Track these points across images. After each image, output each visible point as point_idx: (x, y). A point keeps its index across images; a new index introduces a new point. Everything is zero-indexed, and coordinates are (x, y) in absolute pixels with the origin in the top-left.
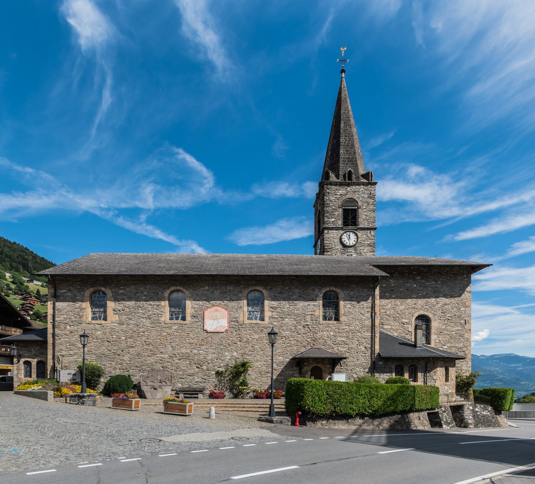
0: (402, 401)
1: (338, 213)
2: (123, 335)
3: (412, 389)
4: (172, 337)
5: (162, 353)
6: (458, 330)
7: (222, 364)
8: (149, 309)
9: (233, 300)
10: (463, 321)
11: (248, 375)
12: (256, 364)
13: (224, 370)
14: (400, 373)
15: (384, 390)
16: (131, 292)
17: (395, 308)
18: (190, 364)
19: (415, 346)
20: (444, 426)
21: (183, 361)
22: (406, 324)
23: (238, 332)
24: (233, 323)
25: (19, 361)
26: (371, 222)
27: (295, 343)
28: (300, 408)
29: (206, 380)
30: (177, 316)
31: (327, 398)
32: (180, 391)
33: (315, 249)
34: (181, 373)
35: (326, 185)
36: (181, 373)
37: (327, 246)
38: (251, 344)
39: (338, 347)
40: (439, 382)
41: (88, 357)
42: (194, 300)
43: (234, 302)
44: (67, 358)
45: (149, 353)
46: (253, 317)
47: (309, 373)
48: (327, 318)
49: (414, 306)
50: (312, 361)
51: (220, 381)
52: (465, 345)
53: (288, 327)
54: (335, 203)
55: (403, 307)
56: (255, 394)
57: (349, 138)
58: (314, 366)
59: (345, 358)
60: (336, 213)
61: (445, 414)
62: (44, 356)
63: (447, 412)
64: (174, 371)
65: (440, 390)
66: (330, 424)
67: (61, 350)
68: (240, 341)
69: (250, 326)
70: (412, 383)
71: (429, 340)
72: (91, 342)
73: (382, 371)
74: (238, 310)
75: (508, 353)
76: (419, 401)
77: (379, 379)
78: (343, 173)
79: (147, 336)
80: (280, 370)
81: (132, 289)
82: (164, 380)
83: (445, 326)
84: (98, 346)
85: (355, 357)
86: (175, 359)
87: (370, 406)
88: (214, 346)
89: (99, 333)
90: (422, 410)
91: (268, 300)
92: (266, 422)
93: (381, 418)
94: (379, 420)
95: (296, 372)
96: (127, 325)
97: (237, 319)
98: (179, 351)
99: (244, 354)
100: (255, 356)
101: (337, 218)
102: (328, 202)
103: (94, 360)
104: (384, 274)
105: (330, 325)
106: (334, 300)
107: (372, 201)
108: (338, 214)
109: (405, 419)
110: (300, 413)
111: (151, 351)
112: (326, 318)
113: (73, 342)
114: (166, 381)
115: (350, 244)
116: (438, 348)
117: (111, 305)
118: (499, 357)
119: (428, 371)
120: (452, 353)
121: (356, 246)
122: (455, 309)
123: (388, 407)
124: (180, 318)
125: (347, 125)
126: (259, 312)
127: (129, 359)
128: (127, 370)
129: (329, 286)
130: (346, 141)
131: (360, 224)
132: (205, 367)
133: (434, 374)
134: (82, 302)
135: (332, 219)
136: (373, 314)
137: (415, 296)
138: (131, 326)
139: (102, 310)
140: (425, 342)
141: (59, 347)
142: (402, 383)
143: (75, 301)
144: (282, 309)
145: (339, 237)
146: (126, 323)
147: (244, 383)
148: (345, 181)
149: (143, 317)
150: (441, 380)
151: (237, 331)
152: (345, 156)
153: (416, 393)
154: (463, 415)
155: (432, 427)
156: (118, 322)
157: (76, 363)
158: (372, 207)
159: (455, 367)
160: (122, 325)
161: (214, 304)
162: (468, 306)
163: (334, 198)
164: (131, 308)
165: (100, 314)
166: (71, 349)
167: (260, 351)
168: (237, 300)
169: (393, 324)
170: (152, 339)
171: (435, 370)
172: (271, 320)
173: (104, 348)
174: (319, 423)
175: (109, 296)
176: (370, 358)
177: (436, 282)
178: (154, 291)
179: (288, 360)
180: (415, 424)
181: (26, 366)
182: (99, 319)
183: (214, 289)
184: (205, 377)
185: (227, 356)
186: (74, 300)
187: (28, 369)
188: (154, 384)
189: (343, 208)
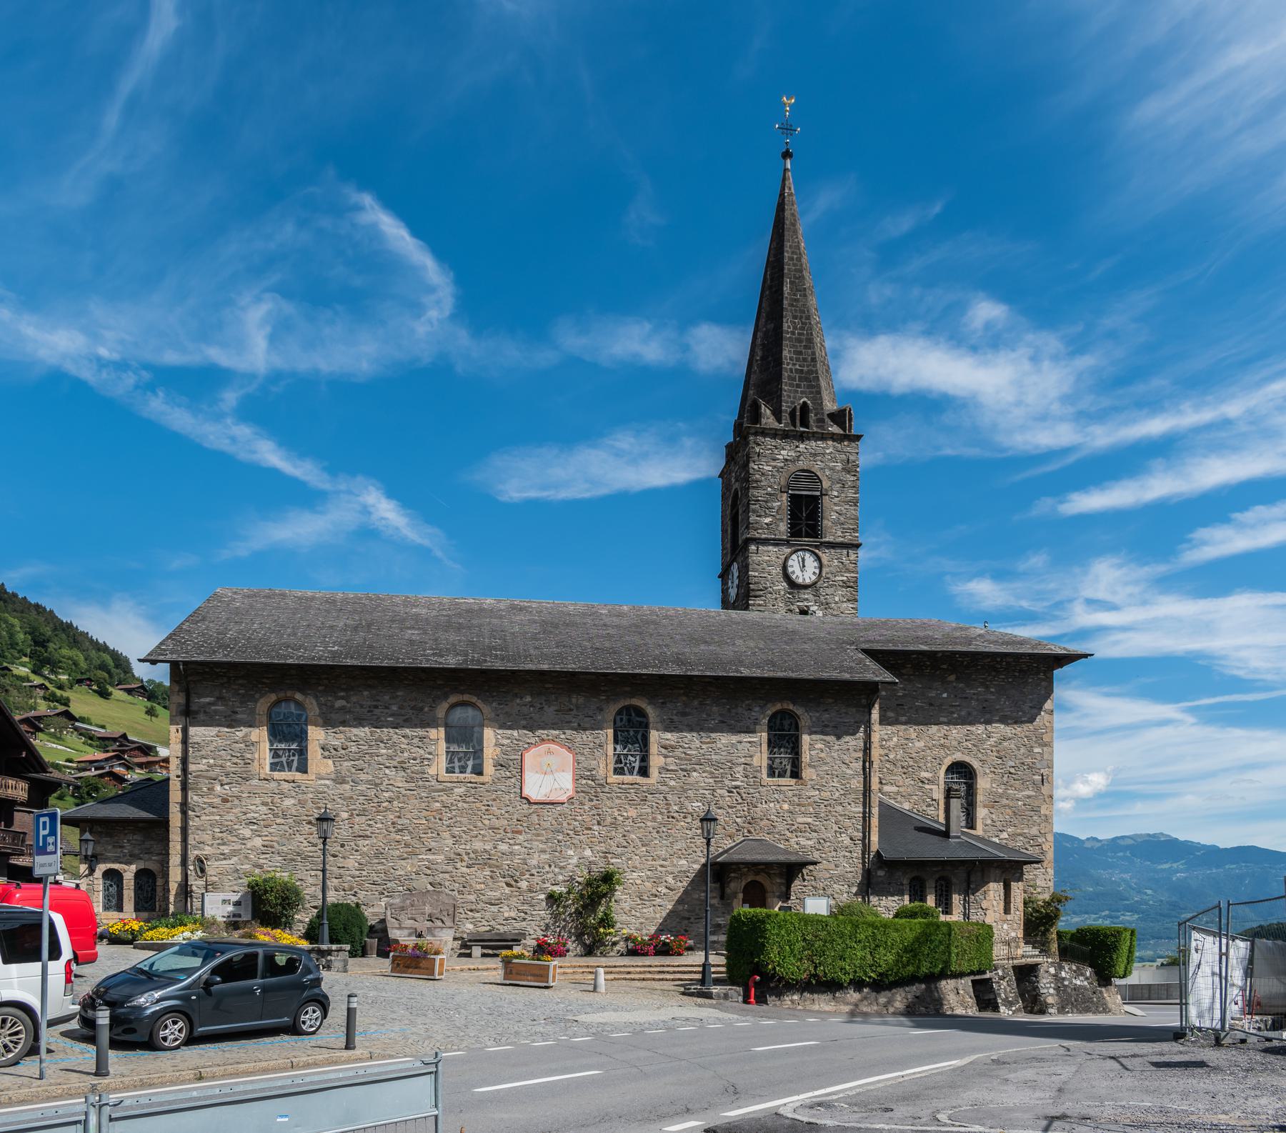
0: (928, 955)
1: (779, 503)
2: (345, 809)
3: (945, 929)
4: (454, 813)
5: (430, 850)
6: (1029, 797)
7: (561, 878)
8: (403, 746)
9: (585, 729)
10: (1038, 778)
11: (616, 901)
12: (631, 877)
13: (564, 890)
14: (918, 895)
15: (897, 930)
16: (362, 706)
17: (905, 747)
18: (492, 877)
19: (946, 834)
20: (1002, 1009)
21: (476, 869)
22: (926, 782)
23: (595, 802)
24: (584, 782)
25: (92, 871)
26: (849, 529)
28: (758, 969)
29: (526, 913)
30: (462, 763)
31: (803, 947)
32: (470, 941)
33: (724, 583)
34: (472, 898)
35: (752, 434)
36: (472, 898)
37: (755, 583)
38: (621, 830)
39: (797, 837)
40: (993, 914)
41: (264, 861)
42: (501, 727)
43: (587, 732)
44: (216, 863)
45: (402, 850)
46: (626, 768)
47: (741, 896)
48: (777, 771)
49: (942, 741)
51: (556, 917)
52: (1042, 832)
54: (772, 480)
55: (921, 744)
56: (631, 945)
57: (802, 323)
59: (815, 863)
60: (775, 504)
61: (1004, 983)
62: (153, 858)
63: (1007, 979)
64: (457, 894)
65: (995, 930)
66: (805, 1000)
67: (201, 843)
68: (599, 824)
69: (619, 788)
70: (943, 918)
71: (972, 819)
72: (271, 823)
73: (884, 892)
75: (1151, 833)
76: (957, 954)
77: (879, 909)
78: (789, 407)
79: (398, 809)
80: (682, 890)
81: (364, 697)
82: (438, 916)
83: (1003, 787)
84: (287, 834)
85: (831, 859)
86: (458, 865)
87: (873, 965)
88: (543, 835)
89: (289, 802)
90: (961, 975)
91: (658, 730)
93: (890, 990)
94: (888, 993)
96: (353, 784)
98: (468, 848)
100: (630, 859)
101: (778, 517)
102: (757, 476)
103: (276, 866)
104: (887, 677)
105: (783, 788)
107: (852, 478)
108: (780, 507)
109: (931, 992)
110: (758, 978)
111: (407, 845)
112: (774, 772)
113: (230, 823)
114: (444, 919)
116: (991, 839)
117: (316, 735)
118: (1130, 842)
119: (973, 889)
120: (1017, 848)
121: (818, 585)
122: (1023, 750)
123: (904, 966)
124: (469, 769)
125: (797, 290)
126: (638, 757)
127: (356, 864)
128: (352, 892)
129: (781, 700)
130: (795, 328)
131: (826, 534)
132: (524, 885)
134: (250, 726)
135: (765, 517)
136: (867, 764)
137: (945, 720)
138: (362, 787)
139: (294, 746)
140: (963, 824)
141: (197, 837)
142: (925, 918)
143: (233, 723)
144: (685, 750)
145: (781, 561)
146: (350, 779)
147: (607, 921)
148: (795, 426)
149: (388, 765)
150: (996, 909)
151: (592, 800)
152: (794, 365)
153: (952, 938)
154: (1037, 987)
155: (980, 1011)
156: (333, 776)
157: (236, 875)
158: (850, 494)
159: (1022, 881)
160: (341, 783)
161: (544, 737)
162: (1048, 745)
163: (770, 468)
164: (362, 742)
165: (289, 756)
166: (226, 840)
167: (640, 845)
168: (593, 729)
169: (901, 784)
170: (410, 817)
171: (985, 888)
173: (302, 840)
174: (787, 999)
175: (312, 714)
177: (987, 687)
178: (414, 703)
179: (697, 867)
180: (950, 1004)
181: (108, 882)
182: (286, 769)
183: (543, 701)
184: (526, 907)
185: (571, 857)
186: (232, 723)
187: (113, 890)
188: (416, 925)
189: (790, 492)
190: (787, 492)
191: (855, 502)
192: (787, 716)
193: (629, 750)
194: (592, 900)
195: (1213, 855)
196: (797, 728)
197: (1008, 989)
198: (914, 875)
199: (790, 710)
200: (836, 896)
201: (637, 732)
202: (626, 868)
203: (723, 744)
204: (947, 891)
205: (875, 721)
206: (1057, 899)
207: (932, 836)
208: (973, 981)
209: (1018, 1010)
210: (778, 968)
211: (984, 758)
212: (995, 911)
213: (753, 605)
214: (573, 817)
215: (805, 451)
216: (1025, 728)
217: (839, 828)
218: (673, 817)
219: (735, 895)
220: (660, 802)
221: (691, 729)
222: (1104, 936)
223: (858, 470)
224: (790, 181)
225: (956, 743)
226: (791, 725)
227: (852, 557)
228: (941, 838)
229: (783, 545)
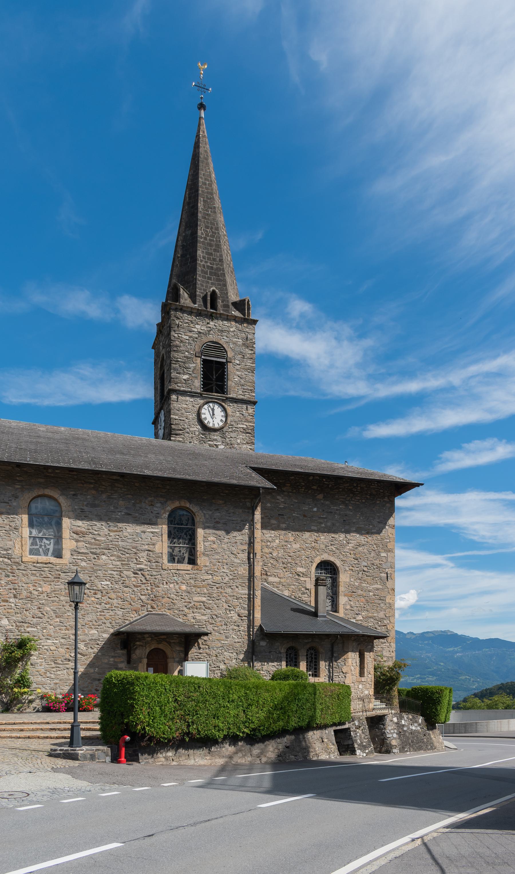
0: (296, 711)
1: (194, 365)
6: (378, 589)
11: (32, 664)
12: (46, 644)
14: (293, 661)
15: (268, 691)
17: (285, 547)
19: (315, 614)
20: (358, 752)
22: (301, 575)
23: (11, 578)
26: (248, 390)
27: (120, 603)
28: (128, 729)
31: (175, 707)
33: (156, 428)
37: (176, 424)
38: (36, 603)
39: (193, 612)
40: (351, 677)
46: (41, 550)
47: (145, 661)
48: (176, 558)
49: (313, 544)
50: (150, 639)
52: (387, 615)
54: (189, 347)
55: (297, 546)
56: (44, 702)
57: (213, 232)
58: (153, 648)
59: (206, 634)
60: (191, 365)
61: (359, 731)
63: (362, 728)
65: (352, 690)
66: (180, 756)
68: (15, 597)
69: (34, 566)
70: (312, 680)
74: (11, 532)
76: (322, 710)
77: (262, 672)
78: (202, 293)
80: (93, 655)
83: (359, 581)
85: (222, 632)
87: (246, 722)
90: (325, 727)
91: (69, 518)
92: (64, 758)
94: (261, 745)
95: (122, 660)
99: (23, 622)
100: (45, 628)
101: (193, 375)
104: (268, 485)
105: (181, 572)
106: (187, 525)
107: (250, 352)
108: (195, 368)
109: (300, 742)
112: (174, 559)
116: (349, 620)
118: (432, 635)
119: (336, 657)
121: (225, 430)
122: (373, 554)
126: (52, 541)
130: (207, 235)
135: (184, 374)
137: (316, 528)
140: (329, 608)
144: (94, 536)
145: (196, 409)
147: (22, 682)
148: (207, 309)
150: (353, 673)
151: (8, 576)
152: (206, 262)
153: (317, 696)
154: (384, 733)
155: (341, 755)
158: (249, 363)
159: (373, 652)
162: (391, 551)
163: (187, 337)
168: (9, 514)
169: (282, 576)
171: (345, 656)
172: (75, 557)
174: (161, 756)
176: (247, 634)
177: (346, 505)
179: (106, 636)
180: (315, 751)
189: (203, 357)
190: (201, 357)
191: (252, 370)
194: (8, 663)
195: (476, 643)
196: (193, 524)
197: (363, 736)
198: (289, 645)
200: (226, 662)
202: (41, 636)
203: (128, 533)
204: (316, 658)
205: (258, 521)
206: (398, 666)
207: (304, 615)
208: (335, 731)
209: (371, 752)
210: (147, 728)
212: (352, 675)
216: (375, 538)
217: (229, 606)
219: (140, 660)
221: (100, 519)
224: (204, 127)
225: (324, 546)
227: (250, 411)
228: (311, 617)
229: (198, 397)
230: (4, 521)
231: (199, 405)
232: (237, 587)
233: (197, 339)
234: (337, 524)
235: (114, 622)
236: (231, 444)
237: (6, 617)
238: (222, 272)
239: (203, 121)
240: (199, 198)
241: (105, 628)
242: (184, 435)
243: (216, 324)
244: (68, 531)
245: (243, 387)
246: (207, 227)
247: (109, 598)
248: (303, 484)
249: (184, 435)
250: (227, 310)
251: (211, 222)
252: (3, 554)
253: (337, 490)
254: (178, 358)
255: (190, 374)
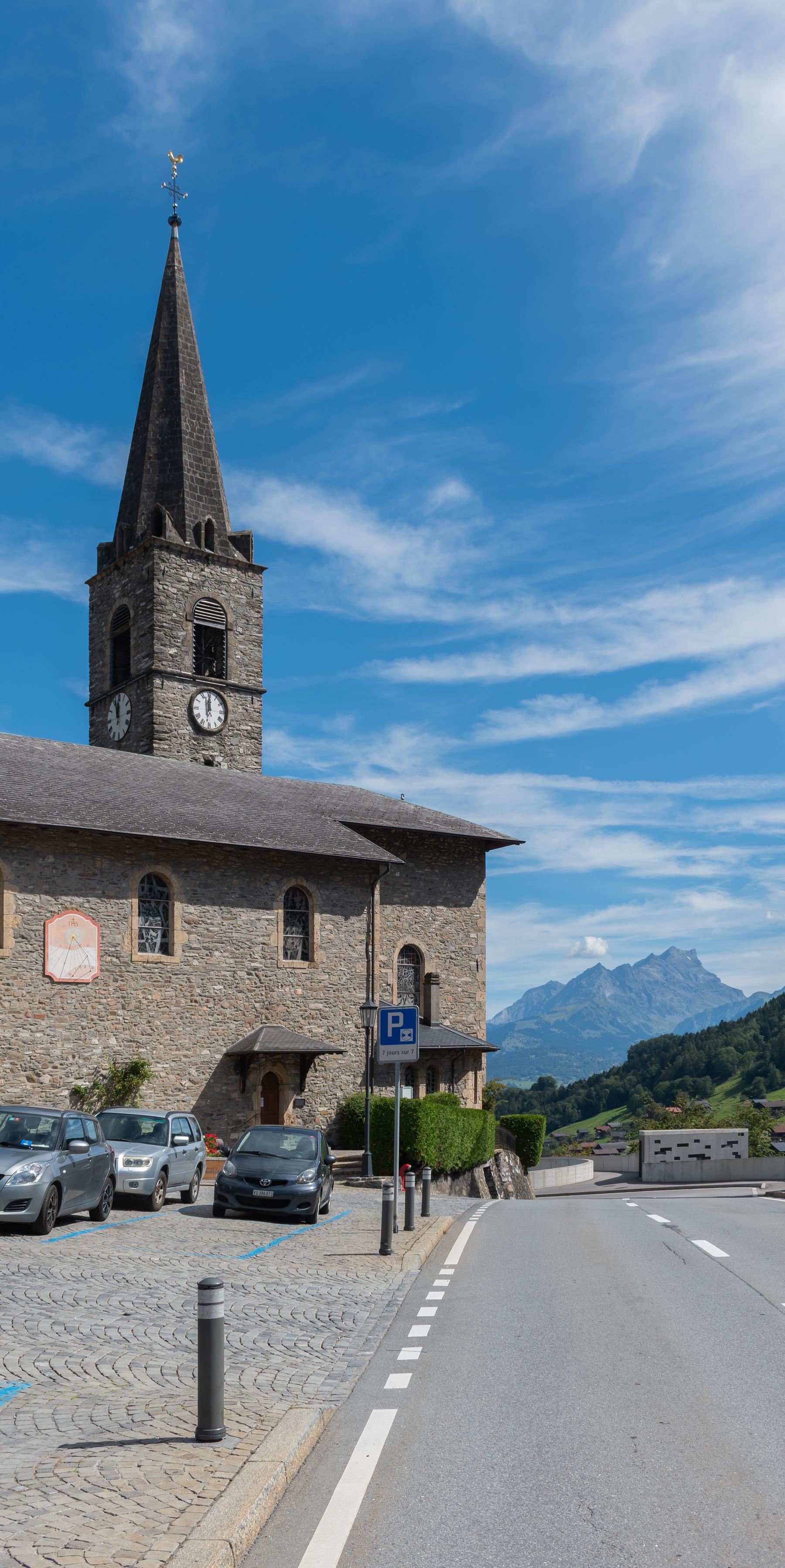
1: (184, 633)
6: (467, 983)
7: (85, 1070)
9: (109, 897)
10: (474, 964)
11: (141, 1097)
18: (12, 1071)
23: (120, 983)
24: (109, 959)
26: (253, 672)
27: (233, 1013)
37: (160, 724)
42: (21, 891)
46: (147, 944)
47: (260, 1088)
48: (289, 952)
49: (396, 923)
52: (477, 1019)
53: (219, 974)
54: (177, 605)
57: (200, 425)
68: (124, 1008)
69: (144, 967)
74: (120, 923)
83: (446, 972)
95: (235, 1088)
97: (118, 949)
99: (131, 1041)
100: (155, 1048)
101: (183, 649)
102: (162, 598)
104: (387, 856)
105: (297, 971)
106: (300, 909)
107: (256, 615)
110: (410, 1166)
115: (209, 725)
121: (223, 733)
126: (159, 933)
130: (193, 429)
132: (46, 1079)
133: (463, 1086)
135: (170, 647)
148: (200, 547)
151: (116, 980)
152: (194, 473)
158: (255, 632)
161: (67, 904)
177: (432, 868)
179: (219, 1057)
189: (195, 621)
190: (192, 621)
192: (298, 894)
193: (151, 924)
199: (303, 887)
200: (343, 1088)
201: (158, 903)
204: (433, 1081)
211: (430, 942)
213: (158, 749)
214: (97, 1000)
215: (211, 576)
216: (463, 912)
217: (346, 1015)
218: (196, 1001)
220: (184, 984)
222: (528, 1125)
223: (262, 606)
224: (178, 254)
226: (301, 902)
227: (257, 705)
229: (189, 682)
230: (112, 908)
231: (190, 695)
232: (355, 989)
233: (187, 593)
234: (422, 895)
235: (226, 1038)
236: (232, 756)
237: (114, 1035)
238: (215, 489)
239: (177, 245)
240: (180, 369)
241: (218, 1047)
242: (170, 741)
243: (213, 572)
244: (180, 920)
245: (247, 668)
246: (193, 417)
247: (222, 1007)
248: (385, 839)
249: (170, 741)
250: (225, 550)
251: (197, 409)
252: (112, 952)
253: (422, 848)
254: (163, 622)
255: (179, 647)
